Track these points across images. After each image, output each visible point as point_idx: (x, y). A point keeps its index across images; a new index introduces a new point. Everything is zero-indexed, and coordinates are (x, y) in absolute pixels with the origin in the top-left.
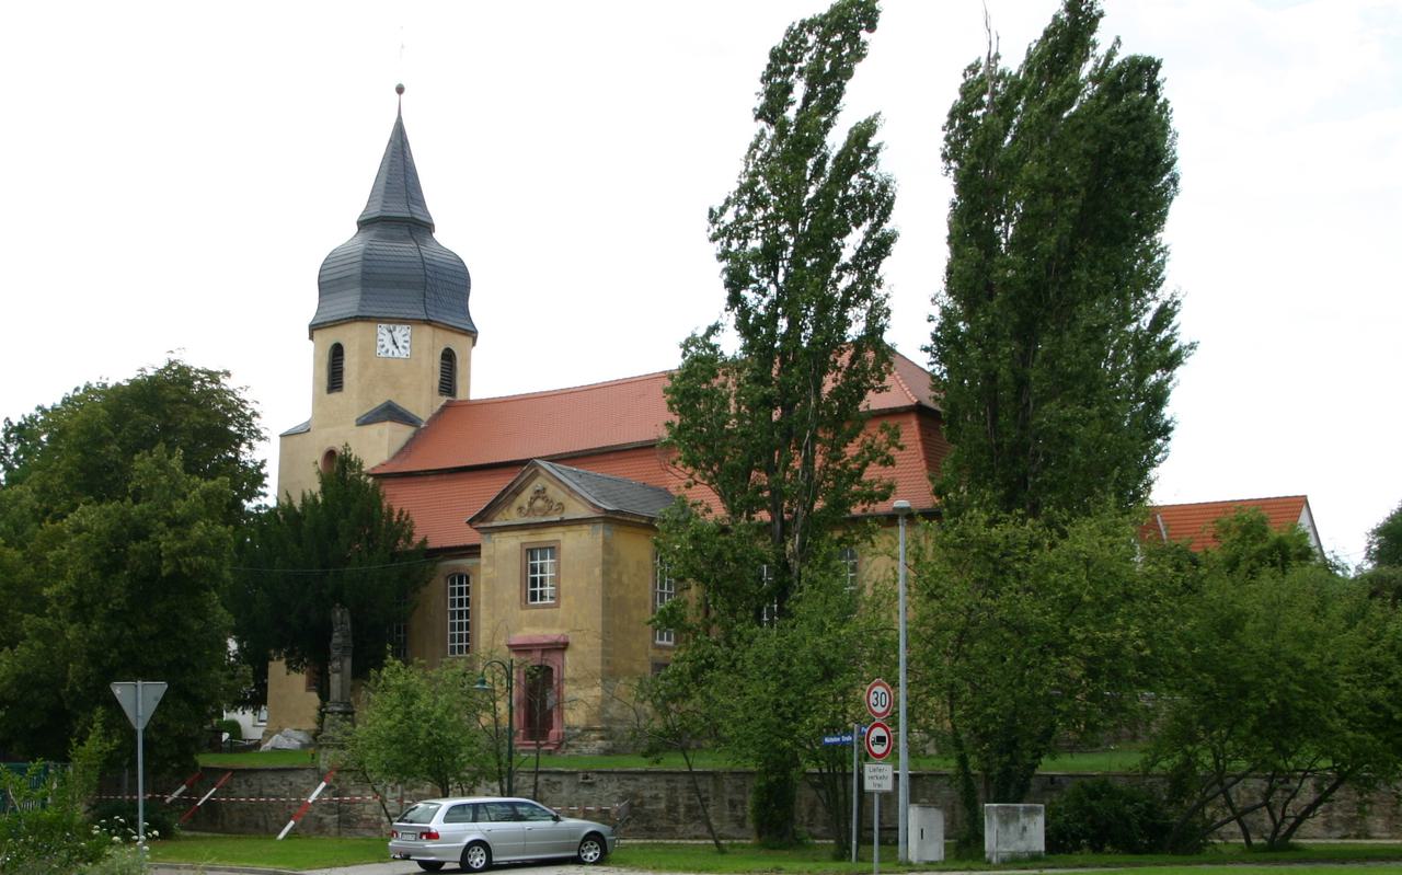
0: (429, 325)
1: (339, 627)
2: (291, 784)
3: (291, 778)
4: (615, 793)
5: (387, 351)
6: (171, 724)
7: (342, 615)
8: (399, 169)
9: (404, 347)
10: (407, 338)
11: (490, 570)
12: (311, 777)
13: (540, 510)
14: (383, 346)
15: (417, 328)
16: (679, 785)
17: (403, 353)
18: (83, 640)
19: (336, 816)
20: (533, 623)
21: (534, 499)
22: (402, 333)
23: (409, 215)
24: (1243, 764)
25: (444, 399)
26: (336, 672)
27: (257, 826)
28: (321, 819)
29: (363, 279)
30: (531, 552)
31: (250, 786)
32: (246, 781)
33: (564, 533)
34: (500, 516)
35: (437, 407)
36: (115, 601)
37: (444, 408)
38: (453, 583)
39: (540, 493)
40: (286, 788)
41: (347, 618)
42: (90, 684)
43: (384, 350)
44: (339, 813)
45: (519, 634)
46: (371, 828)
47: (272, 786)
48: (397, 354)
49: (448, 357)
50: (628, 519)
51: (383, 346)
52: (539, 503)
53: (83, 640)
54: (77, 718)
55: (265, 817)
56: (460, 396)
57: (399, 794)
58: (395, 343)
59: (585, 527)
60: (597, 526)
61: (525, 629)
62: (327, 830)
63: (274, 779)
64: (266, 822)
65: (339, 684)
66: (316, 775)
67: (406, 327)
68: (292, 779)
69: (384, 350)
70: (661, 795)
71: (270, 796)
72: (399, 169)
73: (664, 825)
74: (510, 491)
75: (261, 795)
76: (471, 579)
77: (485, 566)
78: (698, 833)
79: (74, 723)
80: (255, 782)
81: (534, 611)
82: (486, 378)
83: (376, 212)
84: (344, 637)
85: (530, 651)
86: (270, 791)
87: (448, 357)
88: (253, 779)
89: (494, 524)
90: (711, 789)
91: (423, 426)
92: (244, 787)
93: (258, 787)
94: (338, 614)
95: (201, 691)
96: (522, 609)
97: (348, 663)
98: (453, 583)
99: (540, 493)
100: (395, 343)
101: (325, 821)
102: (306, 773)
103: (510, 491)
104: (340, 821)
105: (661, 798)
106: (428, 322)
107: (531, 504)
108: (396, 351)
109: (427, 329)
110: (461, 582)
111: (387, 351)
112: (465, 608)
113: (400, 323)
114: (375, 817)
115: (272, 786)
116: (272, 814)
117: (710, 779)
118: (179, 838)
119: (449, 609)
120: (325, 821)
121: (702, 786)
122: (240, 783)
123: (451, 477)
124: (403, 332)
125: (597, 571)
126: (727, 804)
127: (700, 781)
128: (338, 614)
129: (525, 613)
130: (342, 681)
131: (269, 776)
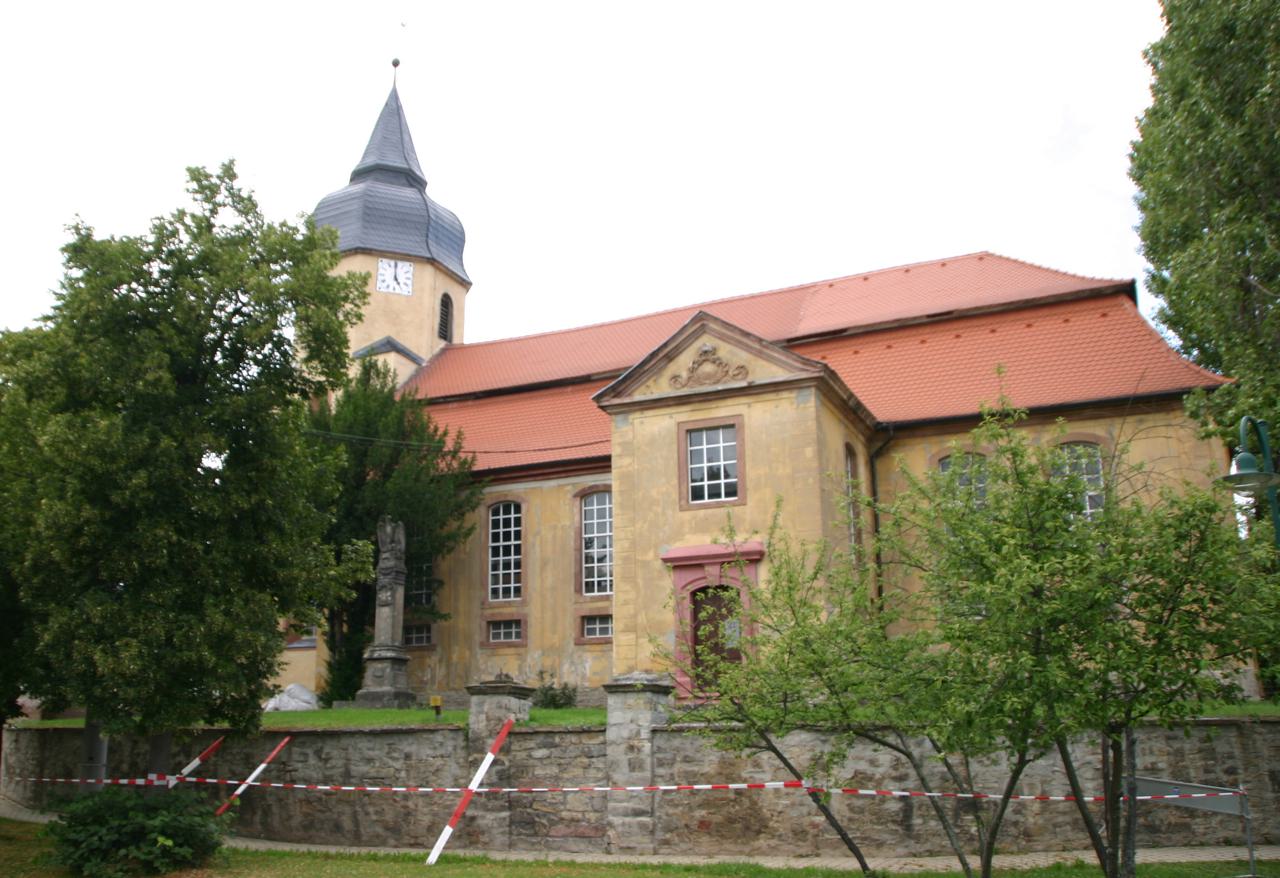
0: (432, 264)
1: (390, 547)
2: (408, 757)
3: (407, 746)
4: (1089, 763)
5: (388, 287)
6: (240, 635)
7: (394, 531)
8: (393, 117)
9: (406, 284)
10: (410, 275)
11: (627, 461)
12: (449, 746)
13: (708, 376)
14: (383, 281)
15: (419, 267)
16: (1187, 746)
17: (405, 290)
18: (75, 446)
19: (505, 814)
20: (701, 528)
21: (698, 364)
22: (405, 269)
23: (405, 166)
24: (1154, 716)
25: (442, 344)
26: (386, 604)
27: (338, 827)
28: (473, 819)
29: (365, 213)
30: (692, 432)
31: (326, 760)
32: (318, 753)
33: (749, 405)
34: (643, 388)
35: (437, 350)
36: (150, 377)
37: (444, 351)
38: (496, 512)
39: (706, 355)
40: (398, 765)
41: (401, 536)
42: (83, 541)
43: (385, 285)
44: (510, 808)
45: (678, 544)
46: (582, 836)
47: (370, 760)
48: (398, 291)
49: (446, 303)
50: (836, 388)
51: (383, 281)
52: (708, 368)
53: (75, 446)
54: (44, 618)
55: (355, 815)
56: (456, 341)
57: (648, 774)
58: (396, 279)
59: (785, 394)
60: (806, 392)
61: (688, 536)
62: (484, 838)
63: (377, 750)
64: (356, 823)
65: (389, 621)
66: (461, 742)
67: (408, 264)
68: (407, 749)
69: (385, 285)
70: (1160, 765)
71: (363, 779)
72: (393, 117)
73: (1173, 820)
74: (661, 355)
75: (347, 777)
76: (524, 508)
77: (620, 456)
78: (1229, 834)
79: (39, 629)
80: (335, 753)
81: (702, 512)
82: (476, 326)
83: (372, 161)
84: (397, 558)
85: (701, 566)
86: (364, 768)
87: (446, 303)
88: (330, 748)
89: (638, 397)
90: (1237, 752)
91: (424, 364)
92: (312, 761)
93: (341, 763)
94: (389, 529)
95: (296, 571)
96: (682, 509)
97: (400, 592)
98: (496, 512)
99: (706, 355)
100: (396, 279)
101: (480, 822)
102: (439, 737)
103: (661, 355)
104: (512, 823)
105: (1162, 770)
106: (432, 262)
107: (692, 370)
108: (397, 287)
109: (429, 270)
110: (507, 511)
111: (388, 287)
112: (513, 542)
113: (403, 260)
114: (592, 816)
115: (370, 760)
116: (371, 809)
117: (1233, 734)
118: (234, 859)
119: (491, 544)
120: (480, 822)
121: (1221, 747)
122: (306, 755)
123: (478, 402)
124: (405, 269)
125: (809, 451)
126: (1267, 779)
127: (1218, 738)
128: (389, 529)
129: (687, 515)
130: (393, 617)
131: (363, 744)
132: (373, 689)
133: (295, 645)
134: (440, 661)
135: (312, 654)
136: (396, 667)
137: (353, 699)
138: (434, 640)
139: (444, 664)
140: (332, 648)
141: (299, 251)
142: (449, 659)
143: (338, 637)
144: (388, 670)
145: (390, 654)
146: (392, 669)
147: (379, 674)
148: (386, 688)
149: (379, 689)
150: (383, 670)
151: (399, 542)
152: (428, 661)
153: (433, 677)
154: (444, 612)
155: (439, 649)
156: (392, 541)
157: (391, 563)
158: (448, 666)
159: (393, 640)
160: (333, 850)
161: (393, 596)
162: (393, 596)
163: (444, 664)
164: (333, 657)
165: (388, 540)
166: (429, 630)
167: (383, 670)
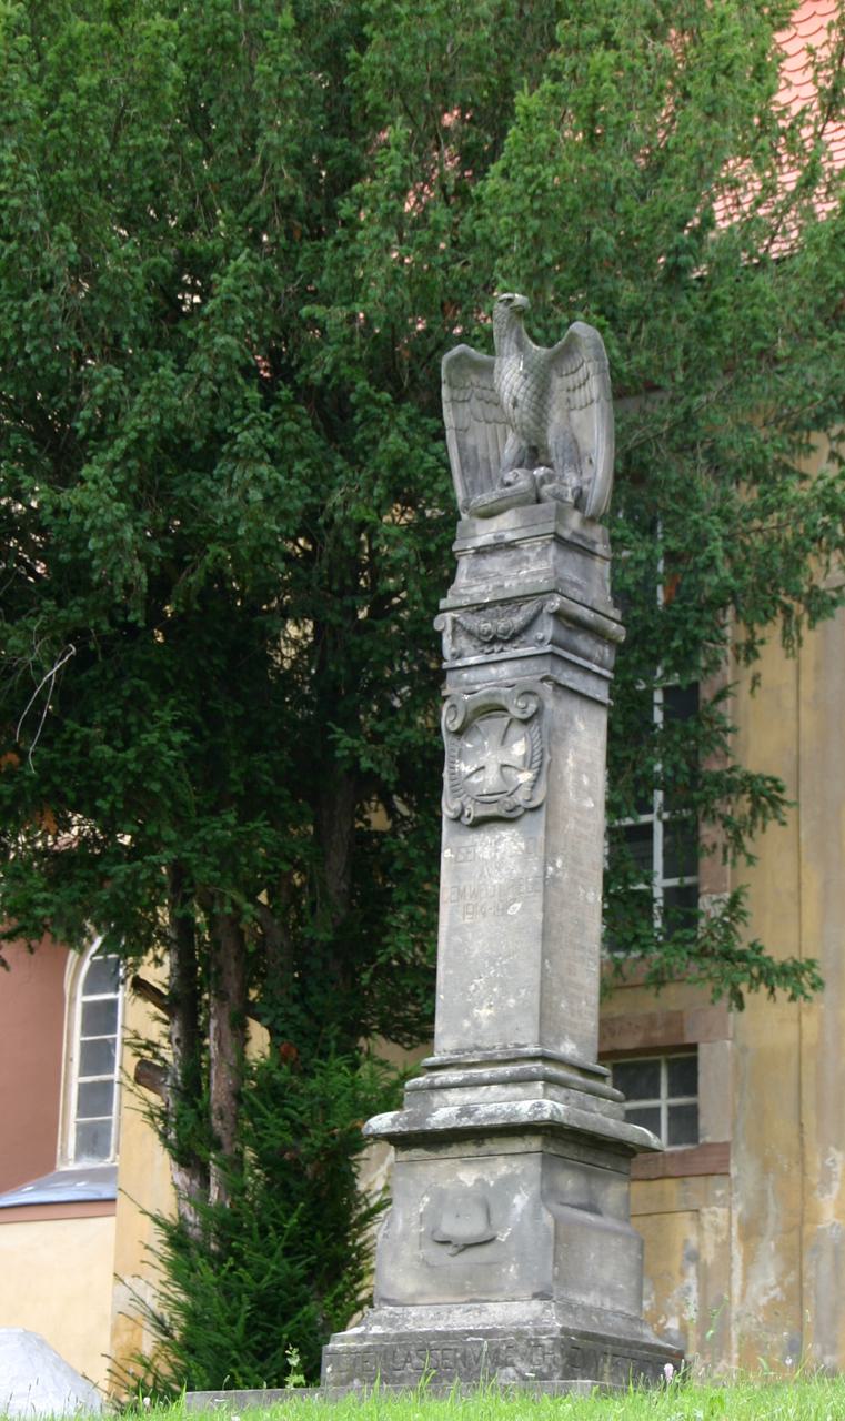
1: (521, 480)
65: (525, 912)
128: (511, 374)
132: (423, 1319)
133: (28, 1195)
134: (751, 1230)
135: (99, 1231)
136: (569, 1182)
137: (312, 1375)
138: (713, 1127)
139: (768, 1246)
140: (187, 1156)
141: (86, 545)
142: (799, 1224)
143: (218, 1088)
144: (520, 1201)
145: (527, 1104)
146: (548, 1194)
147: (468, 1226)
148: (512, 1312)
149: (460, 1319)
150: (489, 1202)
151: (577, 459)
152: (683, 1229)
153: (714, 1310)
154: (778, 951)
155: (742, 1168)
156: (534, 454)
157: (533, 570)
158: (795, 1254)
159: (546, 1019)
160: (59, 1151)
161: (543, 764)
162: (543, 764)
163: (768, 1246)
164: (199, 1200)
165: (511, 447)
166: (686, 1074)
167: (489, 1202)
